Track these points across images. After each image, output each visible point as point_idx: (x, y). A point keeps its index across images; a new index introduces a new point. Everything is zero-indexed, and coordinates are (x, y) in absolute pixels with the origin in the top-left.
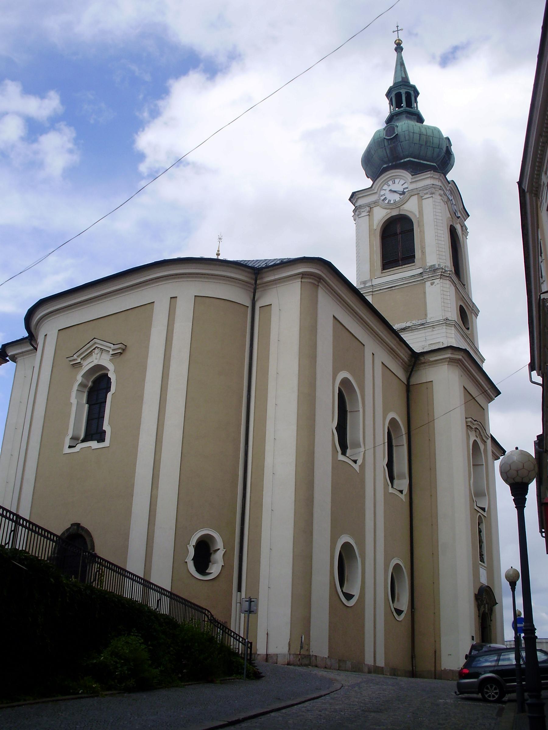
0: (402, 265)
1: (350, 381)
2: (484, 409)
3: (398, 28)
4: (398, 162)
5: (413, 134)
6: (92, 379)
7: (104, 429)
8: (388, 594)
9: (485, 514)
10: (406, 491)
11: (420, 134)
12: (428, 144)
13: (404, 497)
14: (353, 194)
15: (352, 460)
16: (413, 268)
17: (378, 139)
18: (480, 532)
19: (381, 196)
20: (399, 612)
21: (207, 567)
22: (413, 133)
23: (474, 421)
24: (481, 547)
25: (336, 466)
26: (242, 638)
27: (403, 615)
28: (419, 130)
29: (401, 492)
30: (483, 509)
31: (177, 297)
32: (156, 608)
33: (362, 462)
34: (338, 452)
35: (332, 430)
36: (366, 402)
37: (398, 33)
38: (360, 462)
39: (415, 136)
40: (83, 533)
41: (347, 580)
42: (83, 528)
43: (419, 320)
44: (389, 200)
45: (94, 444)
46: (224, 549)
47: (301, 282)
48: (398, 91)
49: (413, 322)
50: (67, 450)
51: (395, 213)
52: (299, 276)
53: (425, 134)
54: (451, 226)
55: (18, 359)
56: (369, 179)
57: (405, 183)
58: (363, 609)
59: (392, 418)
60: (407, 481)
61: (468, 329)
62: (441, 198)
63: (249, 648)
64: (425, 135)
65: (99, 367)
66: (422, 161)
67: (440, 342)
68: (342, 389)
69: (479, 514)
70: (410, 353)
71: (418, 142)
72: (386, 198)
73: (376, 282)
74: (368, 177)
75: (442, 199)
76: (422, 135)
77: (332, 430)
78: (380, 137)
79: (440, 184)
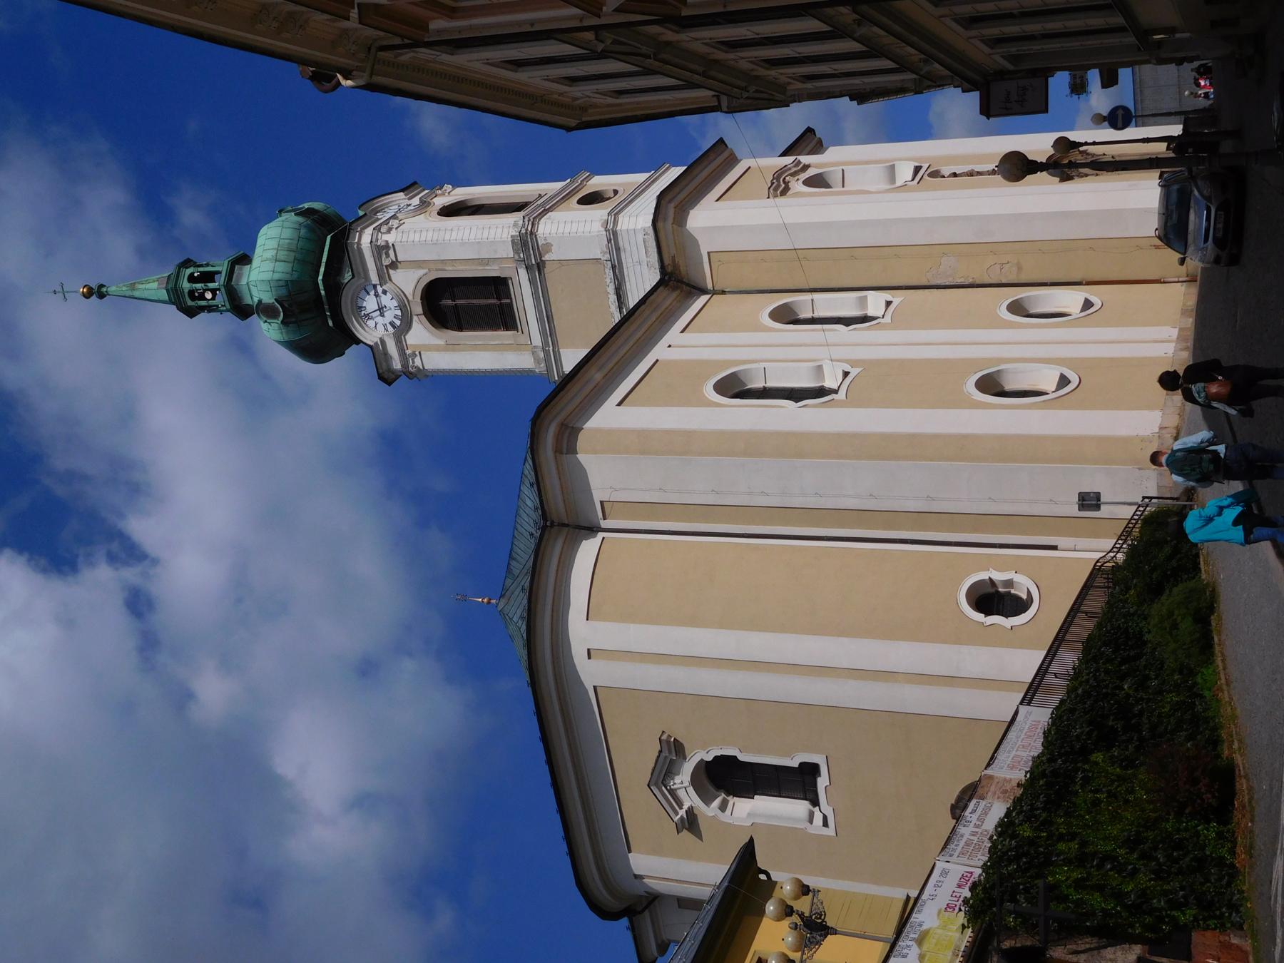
0: (511, 299)
1: (718, 381)
2: (749, 168)
3: (59, 292)
4: (324, 300)
6: (714, 791)
7: (797, 766)
9: (925, 166)
10: (887, 296)
11: (276, 261)
13: (897, 298)
14: (381, 378)
15: (843, 380)
16: (515, 281)
17: (282, 333)
18: (955, 175)
19: (387, 331)
20: (1088, 304)
21: (1018, 598)
22: (274, 272)
23: (774, 185)
24: (979, 174)
25: (850, 402)
26: (1118, 540)
27: (1093, 299)
28: (268, 262)
29: (888, 303)
30: (917, 169)
31: (589, 650)
32: (887, 64)
33: (847, 363)
36: (745, 358)
37: (67, 292)
38: (848, 368)
39: (279, 270)
43: (605, 273)
44: (395, 317)
45: (822, 782)
46: (989, 570)
47: (566, 454)
49: (608, 282)
50: (830, 831)
51: (418, 308)
54: (439, 214)
55: (664, 938)
56: (346, 352)
58: (1083, 360)
59: (770, 317)
60: (871, 295)
61: (616, 192)
62: (394, 230)
64: (277, 253)
65: (695, 781)
66: (324, 260)
67: (644, 239)
68: (731, 393)
69: (926, 177)
70: (661, 288)
72: (390, 323)
73: (537, 340)
74: (344, 354)
75: (397, 228)
76: (278, 257)
78: (280, 329)
79: (369, 231)
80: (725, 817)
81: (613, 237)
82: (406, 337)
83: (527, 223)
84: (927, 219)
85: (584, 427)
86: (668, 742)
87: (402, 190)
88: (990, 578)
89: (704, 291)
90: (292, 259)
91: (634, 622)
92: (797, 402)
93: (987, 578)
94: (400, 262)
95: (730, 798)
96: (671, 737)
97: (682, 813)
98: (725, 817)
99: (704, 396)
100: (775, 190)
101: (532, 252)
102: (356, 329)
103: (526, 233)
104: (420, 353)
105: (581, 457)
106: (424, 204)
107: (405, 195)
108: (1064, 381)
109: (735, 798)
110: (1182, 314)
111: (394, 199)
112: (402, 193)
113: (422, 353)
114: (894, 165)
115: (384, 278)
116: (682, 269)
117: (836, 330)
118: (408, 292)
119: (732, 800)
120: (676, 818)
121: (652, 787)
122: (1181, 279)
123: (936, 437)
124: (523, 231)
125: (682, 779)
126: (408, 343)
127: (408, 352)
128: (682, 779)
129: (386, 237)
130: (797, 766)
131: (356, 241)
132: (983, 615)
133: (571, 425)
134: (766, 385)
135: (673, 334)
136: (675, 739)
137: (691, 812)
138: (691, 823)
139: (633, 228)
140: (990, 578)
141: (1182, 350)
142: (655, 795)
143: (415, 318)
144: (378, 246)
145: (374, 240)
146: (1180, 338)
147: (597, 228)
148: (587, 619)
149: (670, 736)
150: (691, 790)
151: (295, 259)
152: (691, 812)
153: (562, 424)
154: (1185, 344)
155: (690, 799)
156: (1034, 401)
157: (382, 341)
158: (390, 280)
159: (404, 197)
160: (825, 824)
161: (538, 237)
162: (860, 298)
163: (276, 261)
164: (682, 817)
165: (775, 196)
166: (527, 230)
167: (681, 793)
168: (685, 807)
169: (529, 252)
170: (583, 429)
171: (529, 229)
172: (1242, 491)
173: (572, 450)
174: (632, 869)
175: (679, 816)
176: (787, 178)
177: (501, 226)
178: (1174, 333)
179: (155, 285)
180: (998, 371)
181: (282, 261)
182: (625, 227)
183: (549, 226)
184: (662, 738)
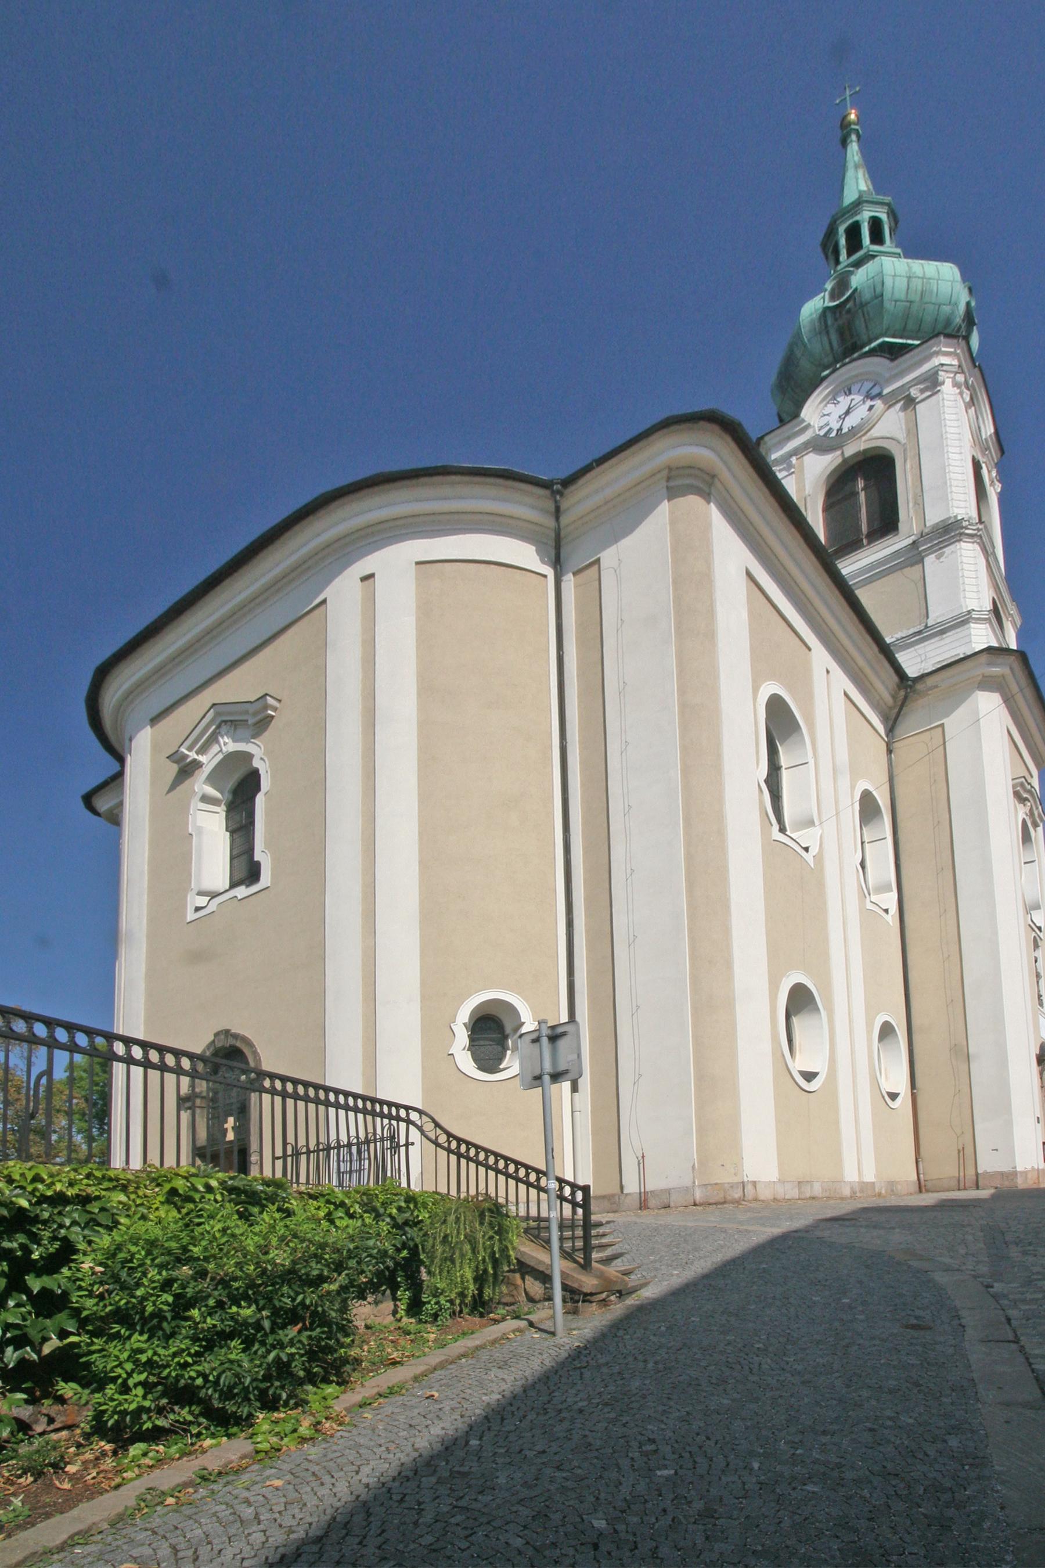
5: (894, 279)
7: (256, 859)
8: (875, 1070)
10: (894, 909)
12: (926, 299)
13: (892, 919)
16: (896, 539)
17: (811, 314)
22: (895, 276)
25: (770, 849)
27: (899, 1100)
29: (886, 911)
34: (772, 825)
35: (759, 785)
38: (814, 851)
40: (238, 1044)
41: (800, 1050)
42: (236, 1036)
47: (667, 487)
48: (850, 221)
50: (191, 916)
52: (658, 476)
53: (921, 275)
57: (875, 385)
60: (894, 895)
63: (580, 1206)
64: (919, 277)
68: (771, 728)
69: (1034, 934)
71: (903, 297)
72: (831, 429)
77: (759, 785)
80: (196, 804)
81: (964, 620)
82: (811, 454)
83: (974, 528)
84: (995, 933)
85: (712, 504)
86: (266, 707)
87: (997, 432)
88: (524, 1023)
89: (890, 730)
90: (911, 297)
91: (418, 619)
92: (765, 781)
93: (523, 1020)
94: (915, 408)
95: (223, 807)
96: (275, 711)
97: (193, 755)
98: (196, 804)
99: (766, 681)
100: (1022, 785)
101: (935, 542)
102: (821, 392)
103: (962, 528)
104: (793, 472)
105: (665, 506)
106: (984, 449)
107: (991, 435)
108: (809, 1076)
109: (224, 813)
110: (889, 1182)
111: (986, 422)
112: (992, 430)
113: (794, 475)
114: (1040, 908)
115: (890, 401)
116: (921, 702)
117: (856, 851)
118: (875, 432)
119: (221, 810)
120: (183, 750)
121: (212, 710)
122: (921, 1176)
123: (727, 931)
124: (964, 524)
125: (228, 744)
126: (805, 458)
127: (794, 460)
128: (228, 744)
129: (948, 382)
130: (256, 859)
131: (943, 349)
132: (466, 1020)
133: (713, 491)
134: (783, 769)
135: (842, 681)
136: (272, 717)
137: (196, 765)
138: (187, 770)
139: (973, 640)
140: (524, 1023)
141: (852, 1188)
142: (204, 717)
143: (839, 452)
144: (936, 373)
145: (945, 368)
146: (864, 1186)
147: (971, 604)
148: (417, 563)
149: (275, 709)
150: (220, 756)
151: (911, 302)
152: (196, 765)
153: (713, 476)
154: (857, 1189)
155: (209, 760)
156: (782, 1044)
157: (808, 426)
158: (890, 407)
159: (989, 434)
160: (198, 909)
161: (957, 543)
162: (891, 885)
163: (909, 278)
164: (187, 756)
165: (1014, 786)
166: (966, 528)
167: (215, 748)
168: (202, 758)
169: (936, 539)
170: (709, 503)
171: (967, 531)
172: (885, 642)
173: (673, 493)
174: (139, 731)
175: (187, 752)
176: (1029, 804)
177: (968, 506)
178: (869, 1177)
179: (863, 187)
180: (818, 1009)
181: (908, 285)
182: (973, 632)
183: (971, 554)
184: (268, 698)
